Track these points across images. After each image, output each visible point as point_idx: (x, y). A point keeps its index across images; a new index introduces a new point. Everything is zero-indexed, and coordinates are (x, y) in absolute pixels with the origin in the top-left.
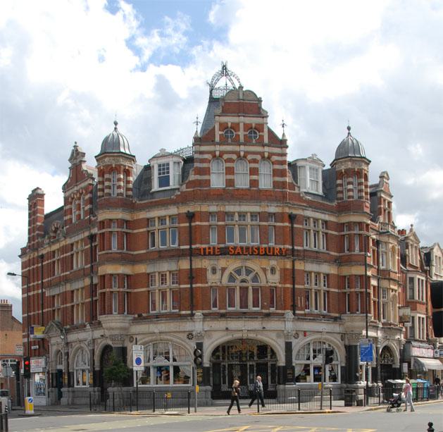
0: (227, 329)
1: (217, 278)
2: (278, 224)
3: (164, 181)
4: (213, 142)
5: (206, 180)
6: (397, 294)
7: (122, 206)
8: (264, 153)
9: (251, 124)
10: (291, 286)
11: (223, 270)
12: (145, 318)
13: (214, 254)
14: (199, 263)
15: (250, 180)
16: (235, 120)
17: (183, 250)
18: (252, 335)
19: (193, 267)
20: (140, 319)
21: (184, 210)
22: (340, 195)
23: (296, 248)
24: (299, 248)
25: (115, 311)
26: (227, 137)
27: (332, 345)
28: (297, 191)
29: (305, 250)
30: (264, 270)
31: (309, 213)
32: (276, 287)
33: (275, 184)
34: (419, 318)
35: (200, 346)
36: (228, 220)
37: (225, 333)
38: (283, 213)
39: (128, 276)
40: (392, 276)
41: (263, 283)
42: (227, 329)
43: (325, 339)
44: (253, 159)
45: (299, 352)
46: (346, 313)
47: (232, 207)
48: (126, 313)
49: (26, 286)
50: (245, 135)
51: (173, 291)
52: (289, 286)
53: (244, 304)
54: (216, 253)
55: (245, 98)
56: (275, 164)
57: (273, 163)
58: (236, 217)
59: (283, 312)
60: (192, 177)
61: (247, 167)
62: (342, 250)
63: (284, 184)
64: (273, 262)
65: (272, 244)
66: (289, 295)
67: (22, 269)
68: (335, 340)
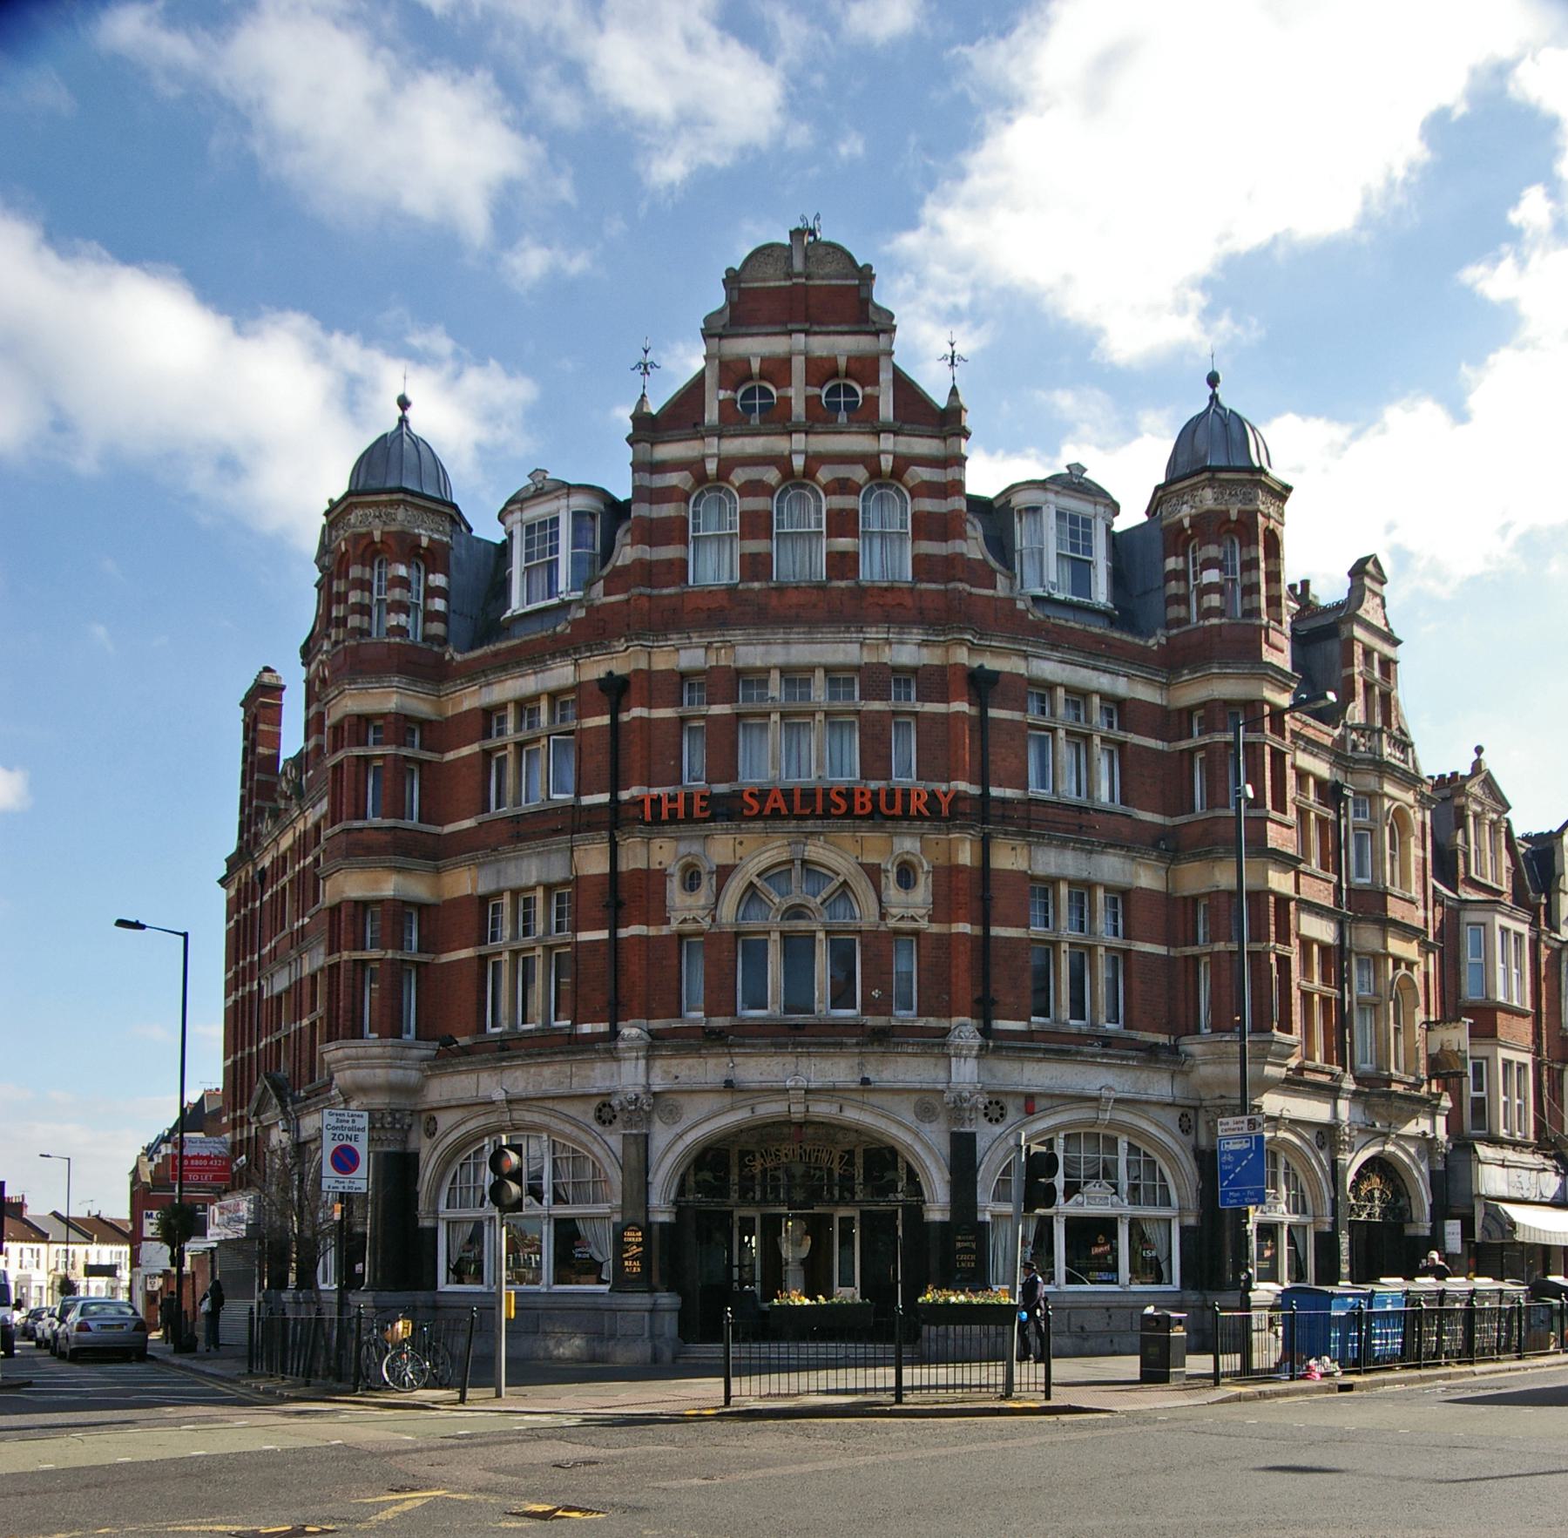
0: (729, 1085)
1: (702, 902)
5: (670, 562)
7: (400, 671)
8: (876, 456)
9: (833, 360)
12: (466, 1051)
13: (690, 819)
16: (777, 345)
18: (823, 1109)
19: (623, 866)
20: (448, 1055)
21: (595, 669)
22: (1176, 611)
24: (1009, 793)
27: (1144, 1148)
28: (1002, 588)
30: (873, 873)
31: (1049, 669)
34: (1507, 1064)
36: (747, 699)
37: (727, 1099)
39: (422, 907)
40: (1395, 910)
41: (865, 913)
42: (729, 1085)
43: (1112, 1124)
44: (838, 480)
46: (1197, 1031)
47: (760, 649)
50: (808, 399)
52: (964, 928)
54: (697, 813)
56: (922, 495)
58: (775, 688)
59: (944, 1023)
60: (626, 554)
61: (819, 511)
63: (951, 567)
64: (908, 845)
65: (909, 781)
66: (962, 963)
68: (1152, 1129)
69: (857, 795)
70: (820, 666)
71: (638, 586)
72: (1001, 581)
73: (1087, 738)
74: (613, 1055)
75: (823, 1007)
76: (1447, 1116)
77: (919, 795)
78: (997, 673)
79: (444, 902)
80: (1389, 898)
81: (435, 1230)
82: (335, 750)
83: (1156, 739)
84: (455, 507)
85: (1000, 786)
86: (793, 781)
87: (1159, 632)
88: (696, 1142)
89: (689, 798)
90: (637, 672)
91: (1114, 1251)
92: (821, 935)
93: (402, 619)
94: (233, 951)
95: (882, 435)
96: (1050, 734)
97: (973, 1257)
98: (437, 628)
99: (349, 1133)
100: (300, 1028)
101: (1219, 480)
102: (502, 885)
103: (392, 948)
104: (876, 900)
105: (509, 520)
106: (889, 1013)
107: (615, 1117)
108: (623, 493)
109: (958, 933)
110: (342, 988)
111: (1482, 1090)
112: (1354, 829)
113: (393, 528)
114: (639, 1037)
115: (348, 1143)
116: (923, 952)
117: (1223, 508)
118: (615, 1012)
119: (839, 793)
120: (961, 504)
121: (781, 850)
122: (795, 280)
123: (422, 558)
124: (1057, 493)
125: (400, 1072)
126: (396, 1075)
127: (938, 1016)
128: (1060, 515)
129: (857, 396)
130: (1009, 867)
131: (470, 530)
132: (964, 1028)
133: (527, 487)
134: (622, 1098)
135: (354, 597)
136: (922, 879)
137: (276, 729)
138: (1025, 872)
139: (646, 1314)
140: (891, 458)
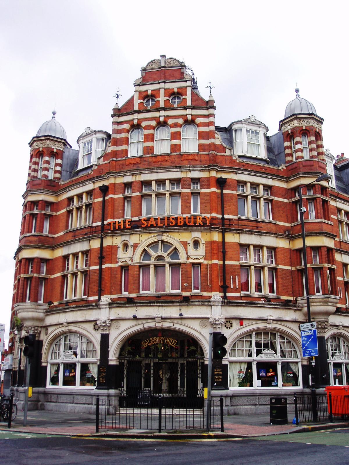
0: (135, 318)
2: (203, 190)
4: (132, 113)
5: (122, 151)
11: (136, 246)
13: (125, 228)
14: (108, 242)
16: (156, 87)
17: (95, 227)
18: (167, 325)
19: (105, 245)
22: (289, 158)
23: (226, 217)
28: (228, 152)
30: (185, 244)
31: (244, 177)
32: (200, 264)
33: (201, 147)
35: (105, 339)
38: (210, 177)
41: (183, 258)
44: (174, 123)
54: (127, 227)
55: (167, 65)
57: (198, 126)
59: (209, 294)
63: (214, 147)
64: (196, 235)
65: (198, 213)
69: (179, 219)
75: (169, 291)
77: (199, 218)
81: (46, 367)
83: (284, 198)
84: (65, 140)
86: (162, 215)
87: (283, 165)
88: (125, 337)
90: (111, 184)
93: (46, 173)
95: (188, 110)
97: (221, 377)
98: (58, 175)
101: (299, 118)
102: (70, 252)
103: (36, 273)
105: (80, 142)
106: (190, 291)
108: (110, 132)
110: (20, 286)
113: (46, 146)
118: (100, 293)
122: (161, 69)
124: (246, 124)
130: (232, 241)
131: (71, 147)
133: (84, 133)
134: (101, 321)
136: (201, 245)
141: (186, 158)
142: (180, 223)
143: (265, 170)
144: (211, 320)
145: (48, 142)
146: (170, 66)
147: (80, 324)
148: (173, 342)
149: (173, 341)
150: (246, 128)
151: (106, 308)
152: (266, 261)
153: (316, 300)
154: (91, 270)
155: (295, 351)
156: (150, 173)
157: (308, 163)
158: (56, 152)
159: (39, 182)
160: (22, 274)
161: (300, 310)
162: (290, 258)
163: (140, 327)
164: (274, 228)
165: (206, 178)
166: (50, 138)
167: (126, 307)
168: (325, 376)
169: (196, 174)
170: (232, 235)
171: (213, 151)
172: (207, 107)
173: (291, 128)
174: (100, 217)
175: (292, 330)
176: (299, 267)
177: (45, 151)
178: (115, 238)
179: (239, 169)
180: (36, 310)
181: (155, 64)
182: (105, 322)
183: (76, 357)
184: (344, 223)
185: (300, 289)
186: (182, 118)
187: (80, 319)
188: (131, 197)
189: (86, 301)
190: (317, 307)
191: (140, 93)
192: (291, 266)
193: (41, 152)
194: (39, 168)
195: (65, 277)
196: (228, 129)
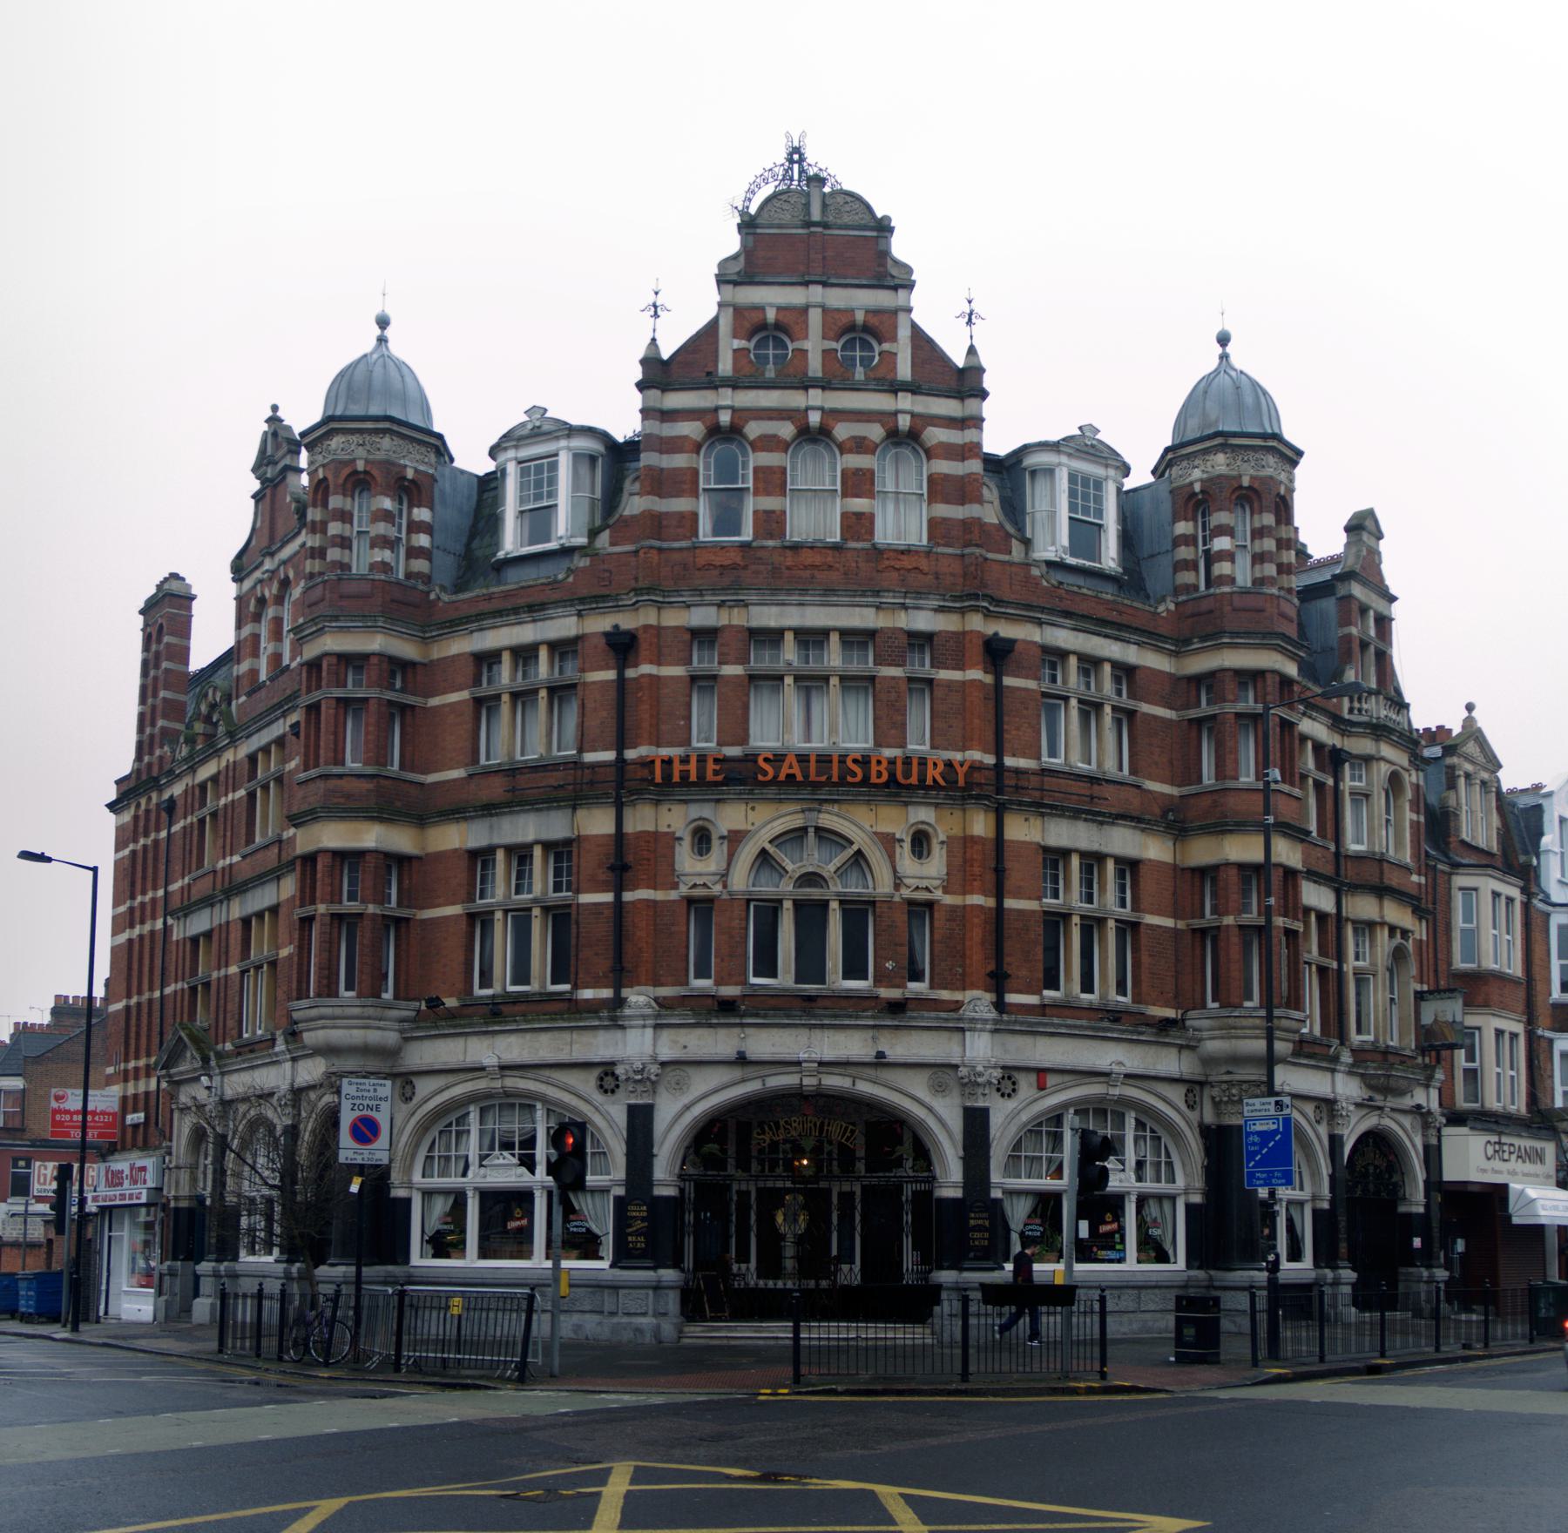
0: (741, 1060)
1: (713, 868)
2: (944, 675)
3: (538, 518)
4: (712, 382)
5: (681, 516)
6: (1410, 945)
10: (990, 902)
11: (735, 839)
12: (452, 1015)
13: (702, 782)
14: (641, 819)
15: (844, 515)
16: (794, 296)
22: (1186, 577)
23: (1009, 761)
25: (349, 987)
26: (763, 360)
29: (1045, 772)
30: (889, 842)
31: (1063, 637)
32: (930, 905)
35: (640, 1122)
38: (964, 633)
41: (882, 885)
45: (1017, 1146)
48: (388, 996)
49: (122, 909)
50: (826, 353)
51: (555, 917)
52: (976, 899)
53: (810, 963)
54: (710, 776)
55: (831, 219)
60: (635, 504)
62: (1190, 773)
63: (969, 526)
64: (923, 814)
65: (918, 745)
66: (977, 934)
67: (117, 850)
69: (874, 762)
70: (835, 629)
71: (649, 538)
72: (1016, 547)
73: (1098, 707)
74: (616, 1024)
76: (1440, 1090)
77: (935, 764)
78: (1013, 642)
79: (427, 855)
80: (1385, 864)
82: (309, 691)
84: (440, 437)
85: (1014, 755)
87: (1169, 599)
89: (702, 759)
90: (647, 628)
91: (1121, 1230)
92: (834, 905)
93: (387, 555)
94: (127, 882)
95: (900, 394)
96: (1062, 703)
97: (986, 1235)
98: (420, 565)
99: (370, 1103)
100: (226, 976)
101: (1232, 445)
102: (496, 841)
103: (374, 902)
104: (890, 870)
105: (502, 457)
107: (617, 1086)
109: (972, 906)
111: (1474, 1061)
112: (1351, 794)
113: (380, 456)
114: (648, 1005)
115: (369, 1113)
116: (936, 923)
117: (1234, 473)
118: (620, 975)
119: (855, 761)
120: (975, 466)
121: (796, 816)
122: (813, 229)
123: (407, 490)
124: (1070, 455)
125: (379, 1033)
126: (374, 1037)
127: (951, 989)
128: (1072, 478)
129: (873, 351)
130: (1023, 838)
132: (979, 1003)
133: (523, 425)
134: (627, 1067)
135: (334, 528)
136: (715, 843)
137: (183, 642)
138: (1038, 844)
139: (651, 1292)
140: (908, 417)
141: (892, 563)
142: (879, 774)
143: (1120, 613)
144: (963, 1071)
145: (386, 442)
146: (839, 221)
147: (547, 1073)
148: (848, 1134)
149: (846, 1128)
150: (1068, 466)
151: (644, 1026)
152: (1109, 900)
153: (1245, 1022)
154: (583, 904)
155: (1170, 1164)
156: (777, 604)
157: (1205, 605)
158: (412, 481)
159: (365, 587)
160: (322, 902)
161: (1192, 1048)
162: (1174, 893)
163: (753, 1087)
164: (1134, 803)
165: (953, 633)
166: (395, 428)
167: (711, 1026)
168: (1266, 1231)
169: (923, 621)
170: (1023, 818)
171: (977, 545)
172: (959, 392)
173: (1205, 476)
174: (611, 734)
175: (1170, 1104)
176: (1197, 923)
177: (375, 472)
178: (664, 808)
179: (1051, 611)
180: (377, 1023)
181: (785, 206)
182: (643, 1069)
183: (532, 1172)
184: (1310, 781)
185: (1198, 988)
186: (879, 421)
187: (563, 1056)
188: (715, 677)
189: (570, 1000)
190: (1247, 1041)
191: (739, 311)
192: (1175, 916)
193: (362, 476)
194: (355, 534)
195: (480, 920)
196: (1007, 464)
